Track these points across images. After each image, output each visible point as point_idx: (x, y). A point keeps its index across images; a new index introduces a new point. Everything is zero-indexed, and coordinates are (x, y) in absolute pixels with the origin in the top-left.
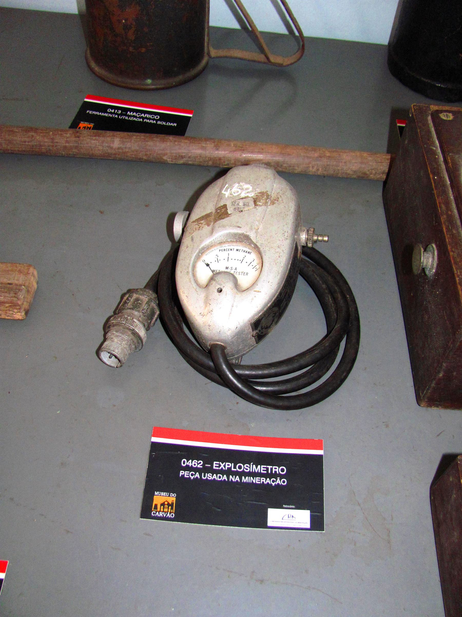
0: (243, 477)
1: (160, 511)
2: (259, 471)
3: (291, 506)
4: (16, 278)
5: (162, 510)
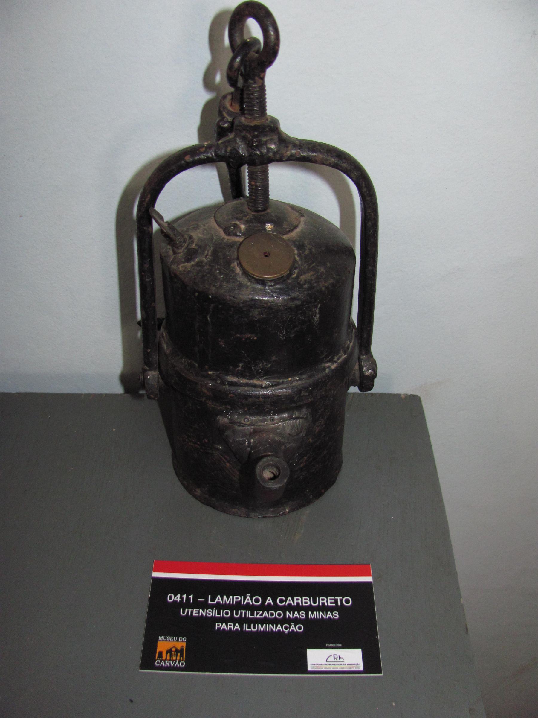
0: (310, 613)
2: (231, 603)
3: (336, 645)
5: (168, 658)
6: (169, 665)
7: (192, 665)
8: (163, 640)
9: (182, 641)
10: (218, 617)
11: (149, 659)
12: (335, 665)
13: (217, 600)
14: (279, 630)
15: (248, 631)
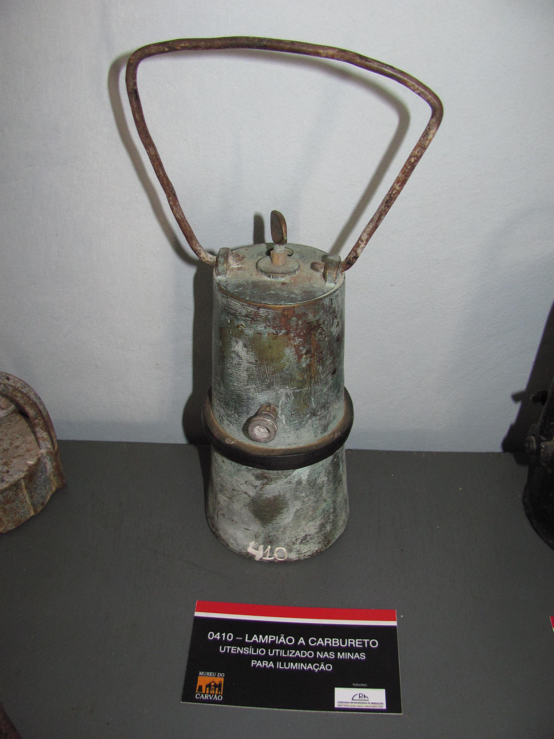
0: (339, 653)
1: (205, 693)
5: (207, 692)
11: (189, 692)
13: (253, 639)
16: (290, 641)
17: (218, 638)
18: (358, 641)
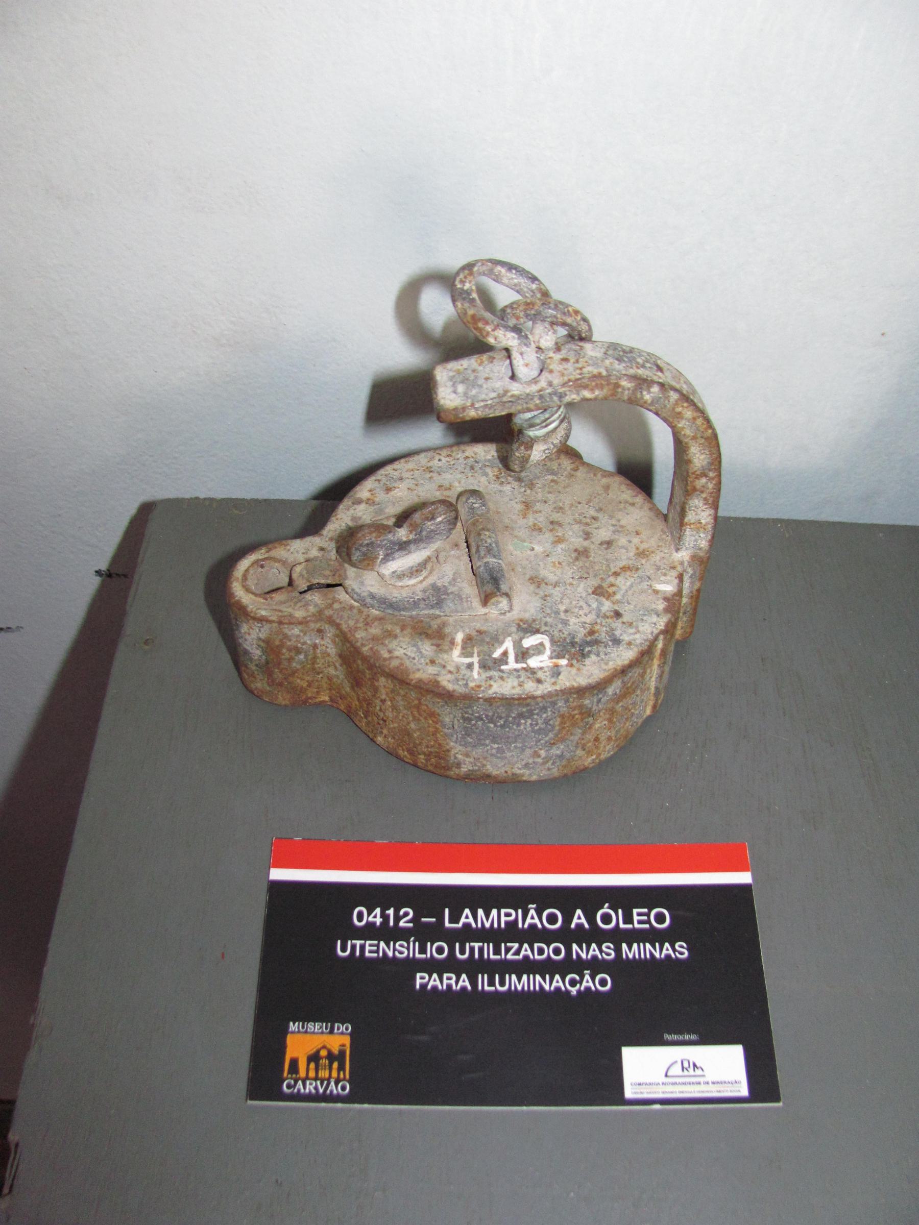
0: (624, 946)
1: (307, 1078)
3: (687, 1037)
4: (529, 642)
6: (313, 1091)
7: (365, 1089)
8: (299, 1032)
9: (342, 1033)
10: (420, 960)
11: (266, 1074)
12: (684, 1084)
13: (463, 920)
14: (558, 989)
15: (489, 993)
16: (552, 919)
17: (378, 920)
18: (639, 914)
